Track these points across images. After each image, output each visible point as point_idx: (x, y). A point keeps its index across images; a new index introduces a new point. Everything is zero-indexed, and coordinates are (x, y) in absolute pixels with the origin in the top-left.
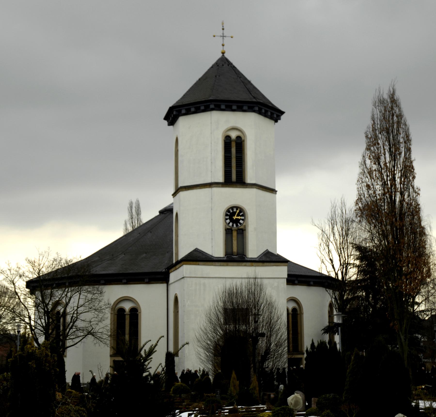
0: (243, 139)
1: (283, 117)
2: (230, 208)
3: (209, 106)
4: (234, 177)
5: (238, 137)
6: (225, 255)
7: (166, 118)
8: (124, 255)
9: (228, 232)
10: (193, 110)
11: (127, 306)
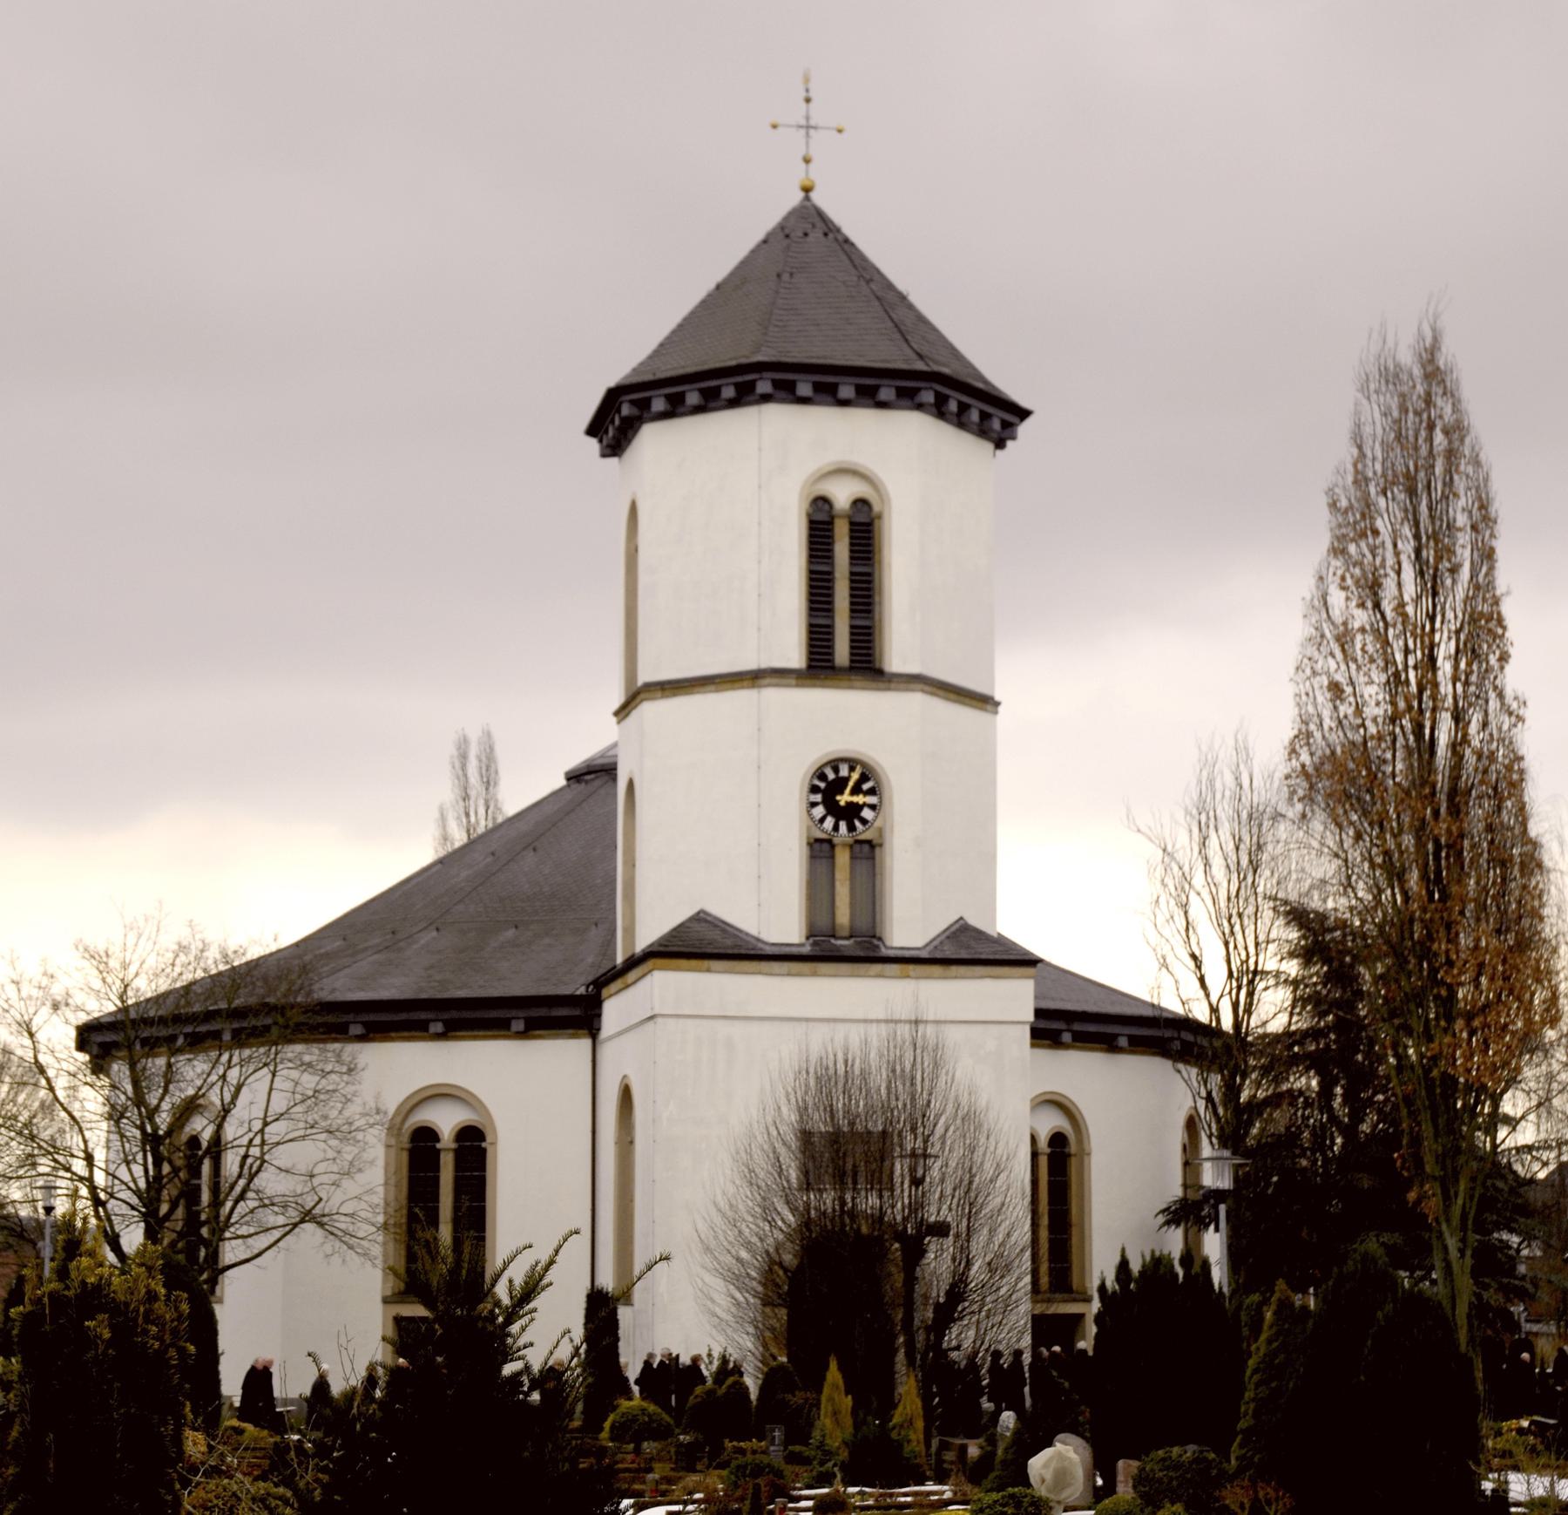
3: (717, 391)
4: (842, 651)
5: (861, 503)
10: (693, 398)
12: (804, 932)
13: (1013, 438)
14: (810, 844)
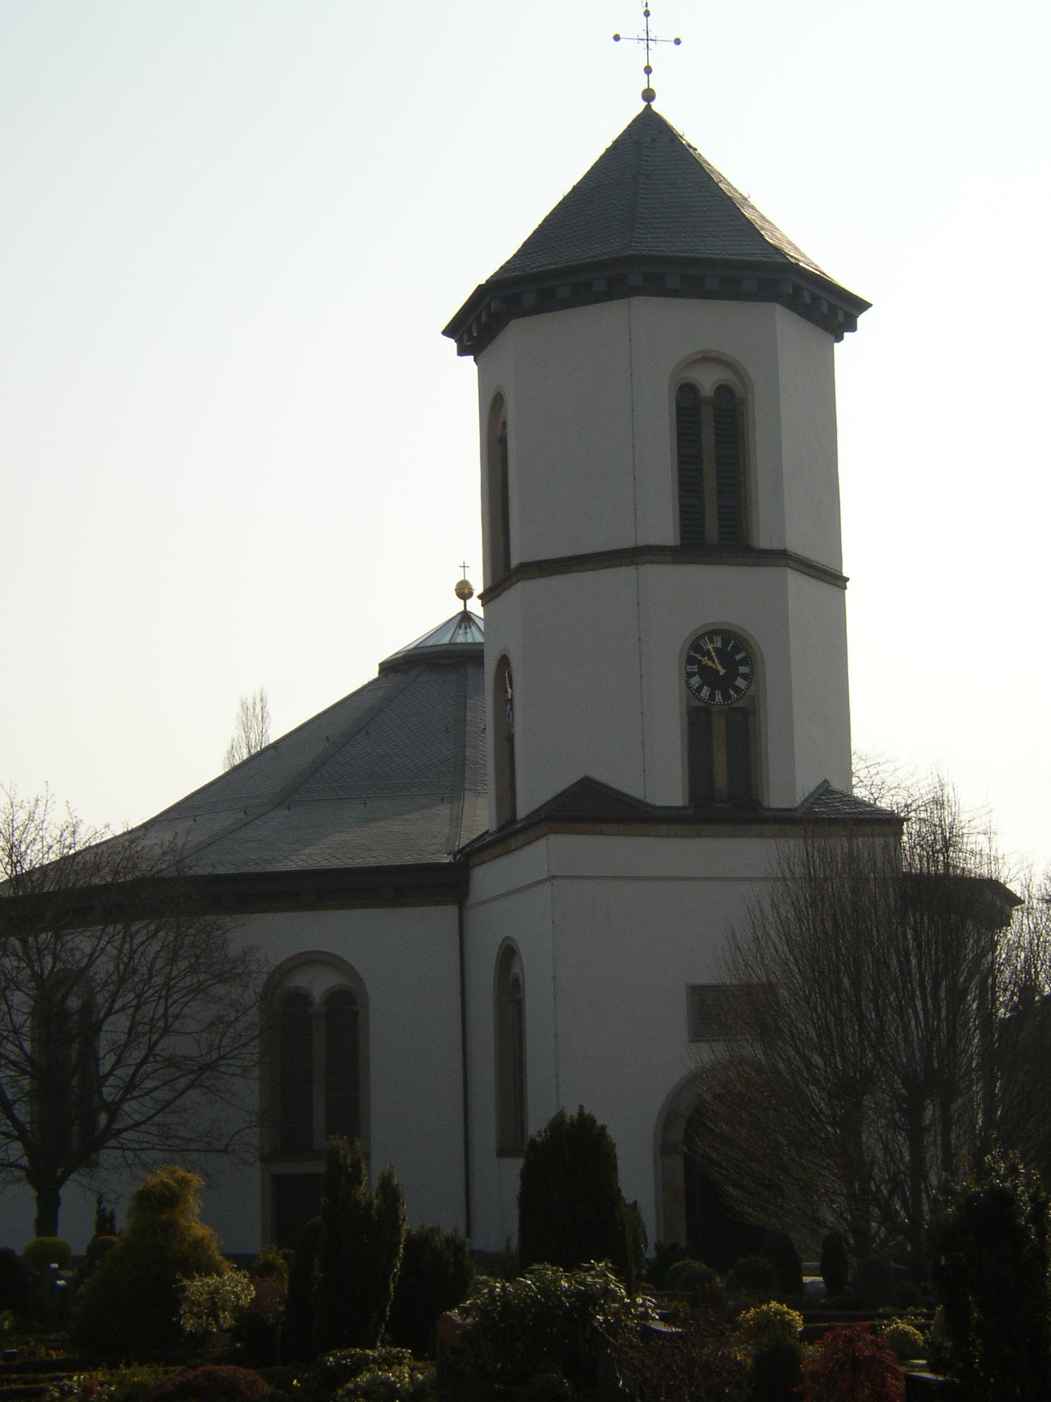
1: (863, 320)
2: (702, 636)
5: (724, 390)
6: (690, 802)
8: (191, 823)
11: (318, 984)
13: (462, 352)
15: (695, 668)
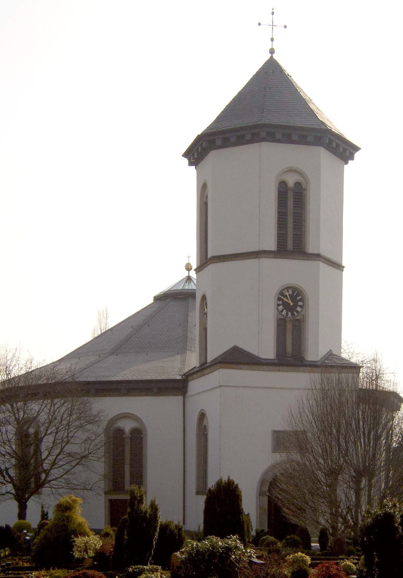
0: (304, 186)
1: (357, 155)
3: (243, 136)
4: (290, 245)
5: (298, 184)
7: (187, 154)
9: (281, 324)
10: (233, 139)
12: (275, 355)
14: (277, 321)
15: (281, 302)
